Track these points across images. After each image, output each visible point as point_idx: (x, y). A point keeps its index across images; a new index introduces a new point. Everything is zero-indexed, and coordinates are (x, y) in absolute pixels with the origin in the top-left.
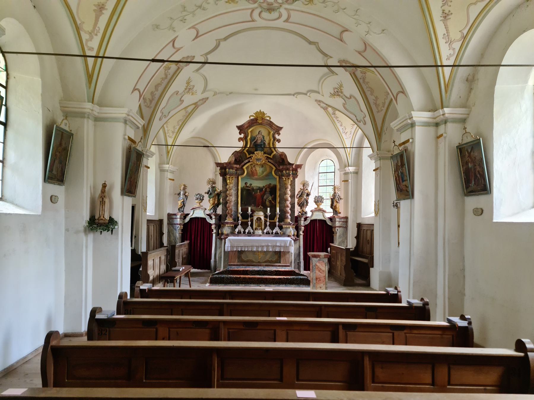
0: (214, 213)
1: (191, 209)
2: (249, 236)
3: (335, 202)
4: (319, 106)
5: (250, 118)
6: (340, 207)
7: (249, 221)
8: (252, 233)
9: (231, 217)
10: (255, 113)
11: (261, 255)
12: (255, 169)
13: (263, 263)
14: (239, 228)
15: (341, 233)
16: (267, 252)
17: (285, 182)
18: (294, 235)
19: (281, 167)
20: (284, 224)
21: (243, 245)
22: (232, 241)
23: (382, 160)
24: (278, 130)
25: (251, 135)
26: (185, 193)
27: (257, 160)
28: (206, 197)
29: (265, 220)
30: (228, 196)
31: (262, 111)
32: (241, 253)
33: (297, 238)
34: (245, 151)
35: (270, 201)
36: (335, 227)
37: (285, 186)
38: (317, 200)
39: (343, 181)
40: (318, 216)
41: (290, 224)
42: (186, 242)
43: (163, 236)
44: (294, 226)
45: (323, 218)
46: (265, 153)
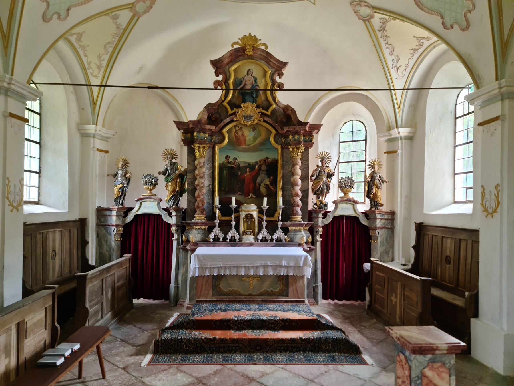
0: (174, 206)
1: (136, 199)
2: (232, 245)
3: (374, 186)
4: (354, 14)
5: (232, 47)
6: (382, 195)
7: (233, 220)
8: (237, 240)
10: (242, 38)
11: (254, 283)
12: (242, 134)
13: (258, 296)
14: (217, 231)
15: (384, 238)
16: (265, 277)
18: (307, 243)
19: (286, 129)
20: (290, 225)
21: (221, 266)
22: (202, 259)
23: (507, 102)
24: (280, 68)
25: (235, 75)
26: (126, 173)
28: (162, 179)
29: (259, 217)
30: (198, 177)
32: (218, 278)
33: (312, 247)
34: (225, 103)
35: (267, 187)
36: (375, 229)
37: (293, 162)
38: (344, 184)
39: (385, 153)
40: (345, 210)
41: (301, 225)
42: (127, 257)
43: (87, 246)
44: (308, 228)
45: (354, 214)
46: (258, 107)
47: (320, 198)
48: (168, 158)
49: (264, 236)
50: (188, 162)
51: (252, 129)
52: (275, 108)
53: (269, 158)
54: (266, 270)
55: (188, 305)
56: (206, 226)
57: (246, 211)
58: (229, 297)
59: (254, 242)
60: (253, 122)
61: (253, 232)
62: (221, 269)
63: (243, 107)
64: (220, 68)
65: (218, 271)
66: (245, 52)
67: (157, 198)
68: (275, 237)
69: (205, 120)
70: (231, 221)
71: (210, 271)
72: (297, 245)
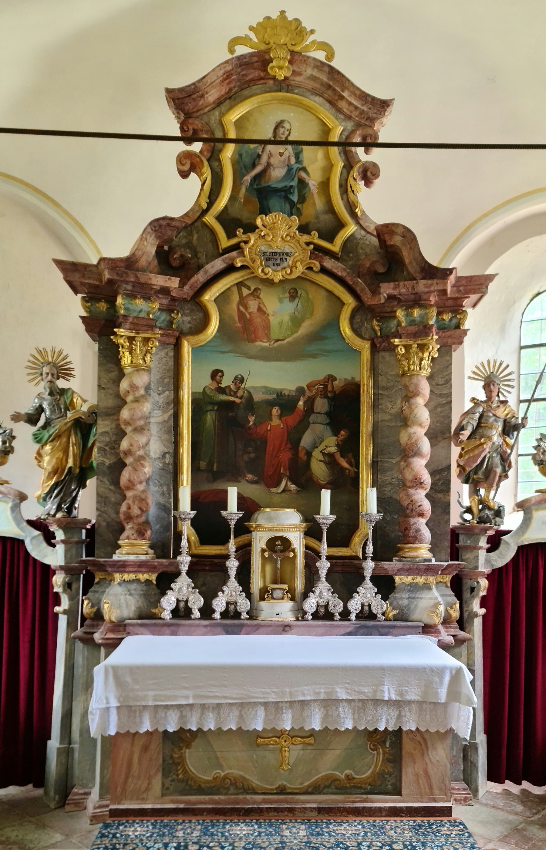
0: (59, 515)
7: (233, 554)
8: (244, 615)
9: (141, 534)
10: (259, 24)
12: (260, 309)
17: (405, 363)
18: (446, 622)
20: (400, 571)
21: (191, 701)
22: (129, 679)
27: (268, 260)
29: (307, 547)
30: (129, 430)
31: (290, 17)
34: (210, 219)
37: (406, 387)
41: (430, 570)
44: (448, 579)
46: (304, 229)
47: (482, 492)
48: (44, 376)
49: (322, 602)
50: (99, 386)
51: (287, 295)
52: (352, 235)
53: (335, 379)
54: (330, 713)
55: (95, 808)
56: (153, 572)
57: (270, 530)
58: (216, 797)
59: (294, 619)
60: (291, 272)
61: (291, 591)
62: (191, 710)
63: (263, 228)
64: (195, 115)
65: (182, 717)
66: (269, 70)
67: (12, 492)
68: (355, 605)
69: (150, 259)
70: (227, 557)
71: (154, 719)
72: (420, 630)
